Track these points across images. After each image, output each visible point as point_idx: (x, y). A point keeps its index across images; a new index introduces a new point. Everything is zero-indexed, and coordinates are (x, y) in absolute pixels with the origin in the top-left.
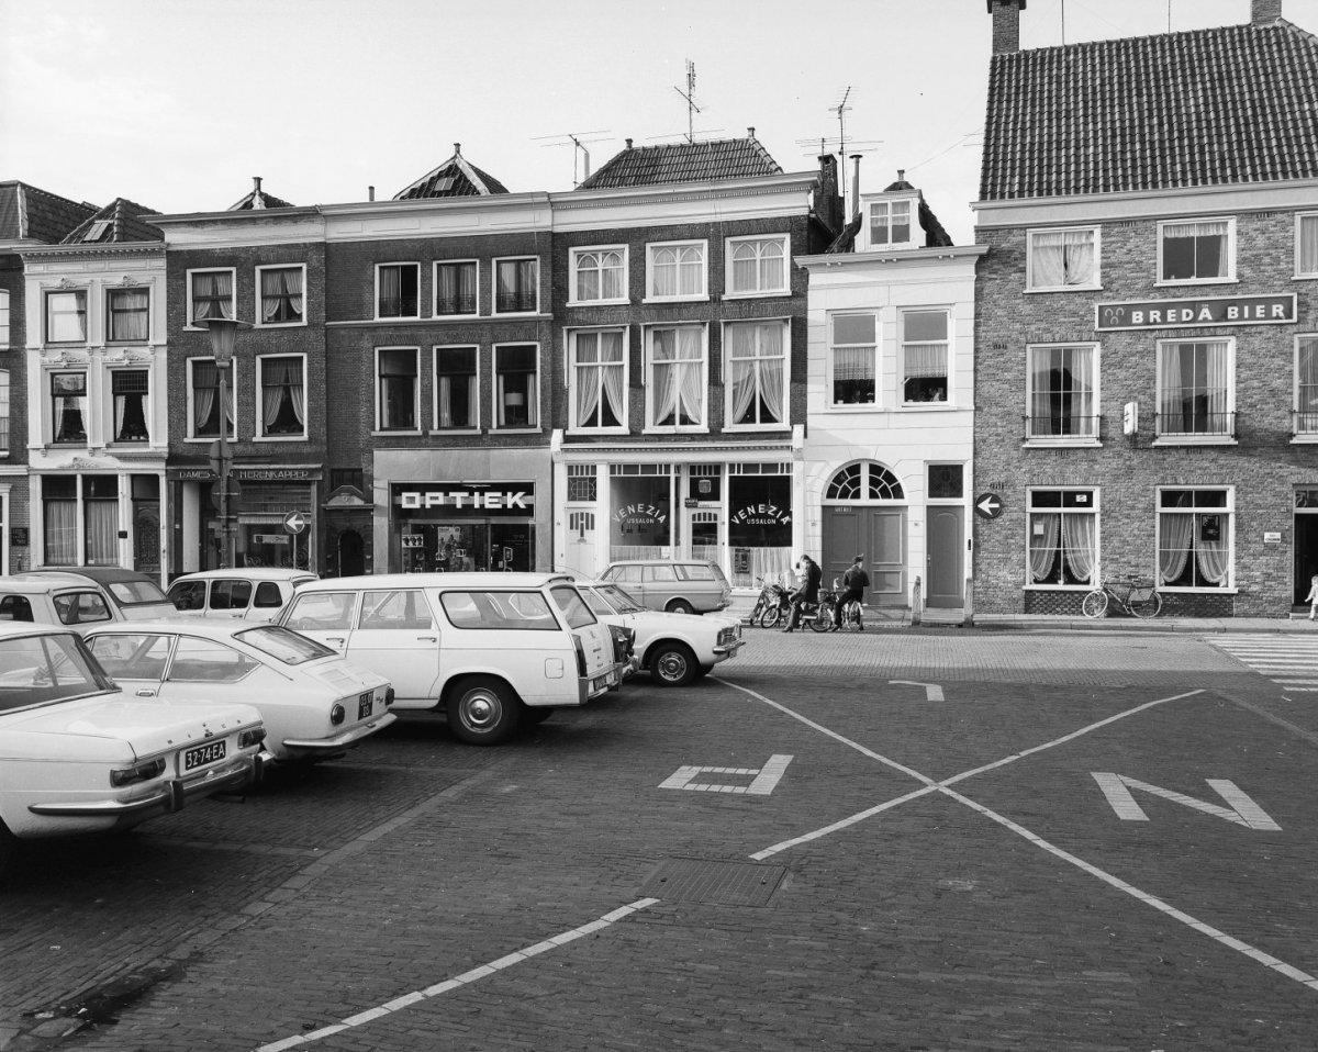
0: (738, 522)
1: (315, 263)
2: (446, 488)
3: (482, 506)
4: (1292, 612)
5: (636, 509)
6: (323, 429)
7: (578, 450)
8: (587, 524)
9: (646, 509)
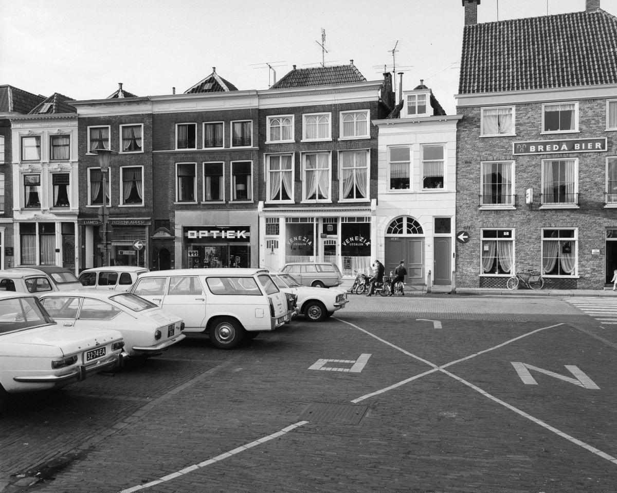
0: (345, 245)
1: (147, 123)
2: (209, 229)
3: (226, 237)
4: (605, 287)
5: (298, 239)
6: (151, 201)
7: (271, 211)
8: (275, 245)
9: (302, 238)
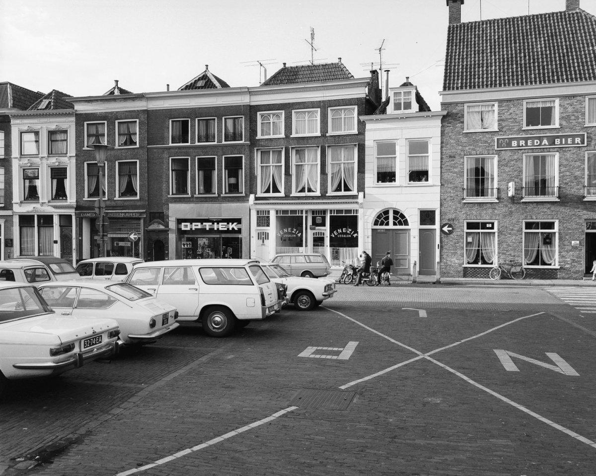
0: (334, 236)
1: (142, 119)
2: (202, 221)
3: (218, 229)
4: (584, 277)
5: (288, 230)
6: (146, 194)
7: (261, 204)
8: (265, 237)
9: (292, 230)
